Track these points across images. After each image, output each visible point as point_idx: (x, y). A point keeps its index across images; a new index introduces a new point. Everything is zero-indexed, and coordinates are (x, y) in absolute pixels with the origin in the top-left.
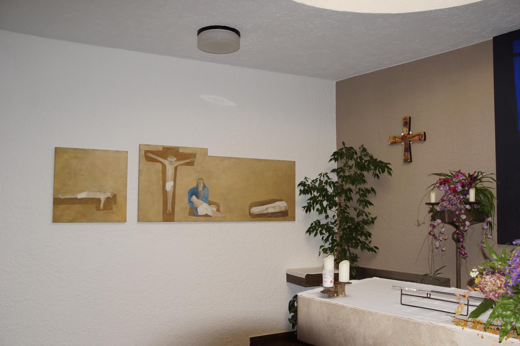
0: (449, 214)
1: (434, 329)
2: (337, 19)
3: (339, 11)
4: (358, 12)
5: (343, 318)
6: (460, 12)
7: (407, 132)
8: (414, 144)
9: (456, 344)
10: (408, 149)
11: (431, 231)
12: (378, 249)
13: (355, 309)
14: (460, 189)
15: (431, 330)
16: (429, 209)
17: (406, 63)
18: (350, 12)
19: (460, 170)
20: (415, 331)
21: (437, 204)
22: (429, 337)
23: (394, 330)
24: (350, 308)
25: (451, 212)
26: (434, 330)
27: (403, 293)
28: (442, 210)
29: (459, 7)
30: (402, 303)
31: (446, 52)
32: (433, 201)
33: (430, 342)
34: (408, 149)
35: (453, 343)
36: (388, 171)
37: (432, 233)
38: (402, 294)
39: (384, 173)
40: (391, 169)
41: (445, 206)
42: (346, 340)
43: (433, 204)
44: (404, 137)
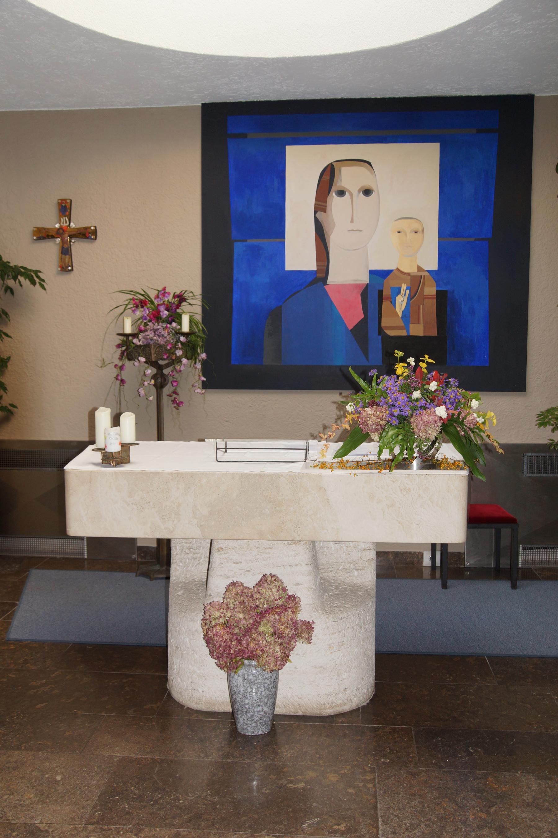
0: (156, 349)
1: (297, 478)
2: (20, 16)
3: (34, 5)
4: (62, 17)
5: (157, 489)
6: (193, 61)
7: (66, 223)
8: (76, 243)
9: (325, 489)
10: (66, 251)
11: (118, 375)
12: (15, 407)
13: (178, 474)
14: (166, 315)
15: (294, 480)
16: (120, 342)
17: (63, 110)
18: (50, 13)
19: (165, 288)
20: (271, 485)
21: (134, 335)
22: (290, 488)
23: (241, 490)
24: (169, 474)
25: (159, 347)
26: (297, 479)
27: (218, 447)
28: (145, 344)
29: (198, 54)
30: (218, 460)
31: (131, 107)
32: (128, 329)
33: (291, 494)
34: (66, 251)
35: (320, 488)
36: (40, 284)
37: (120, 378)
38: (217, 449)
39: (36, 286)
40: (44, 281)
41: (152, 337)
42: (164, 517)
43: (127, 336)
44: (61, 231)
